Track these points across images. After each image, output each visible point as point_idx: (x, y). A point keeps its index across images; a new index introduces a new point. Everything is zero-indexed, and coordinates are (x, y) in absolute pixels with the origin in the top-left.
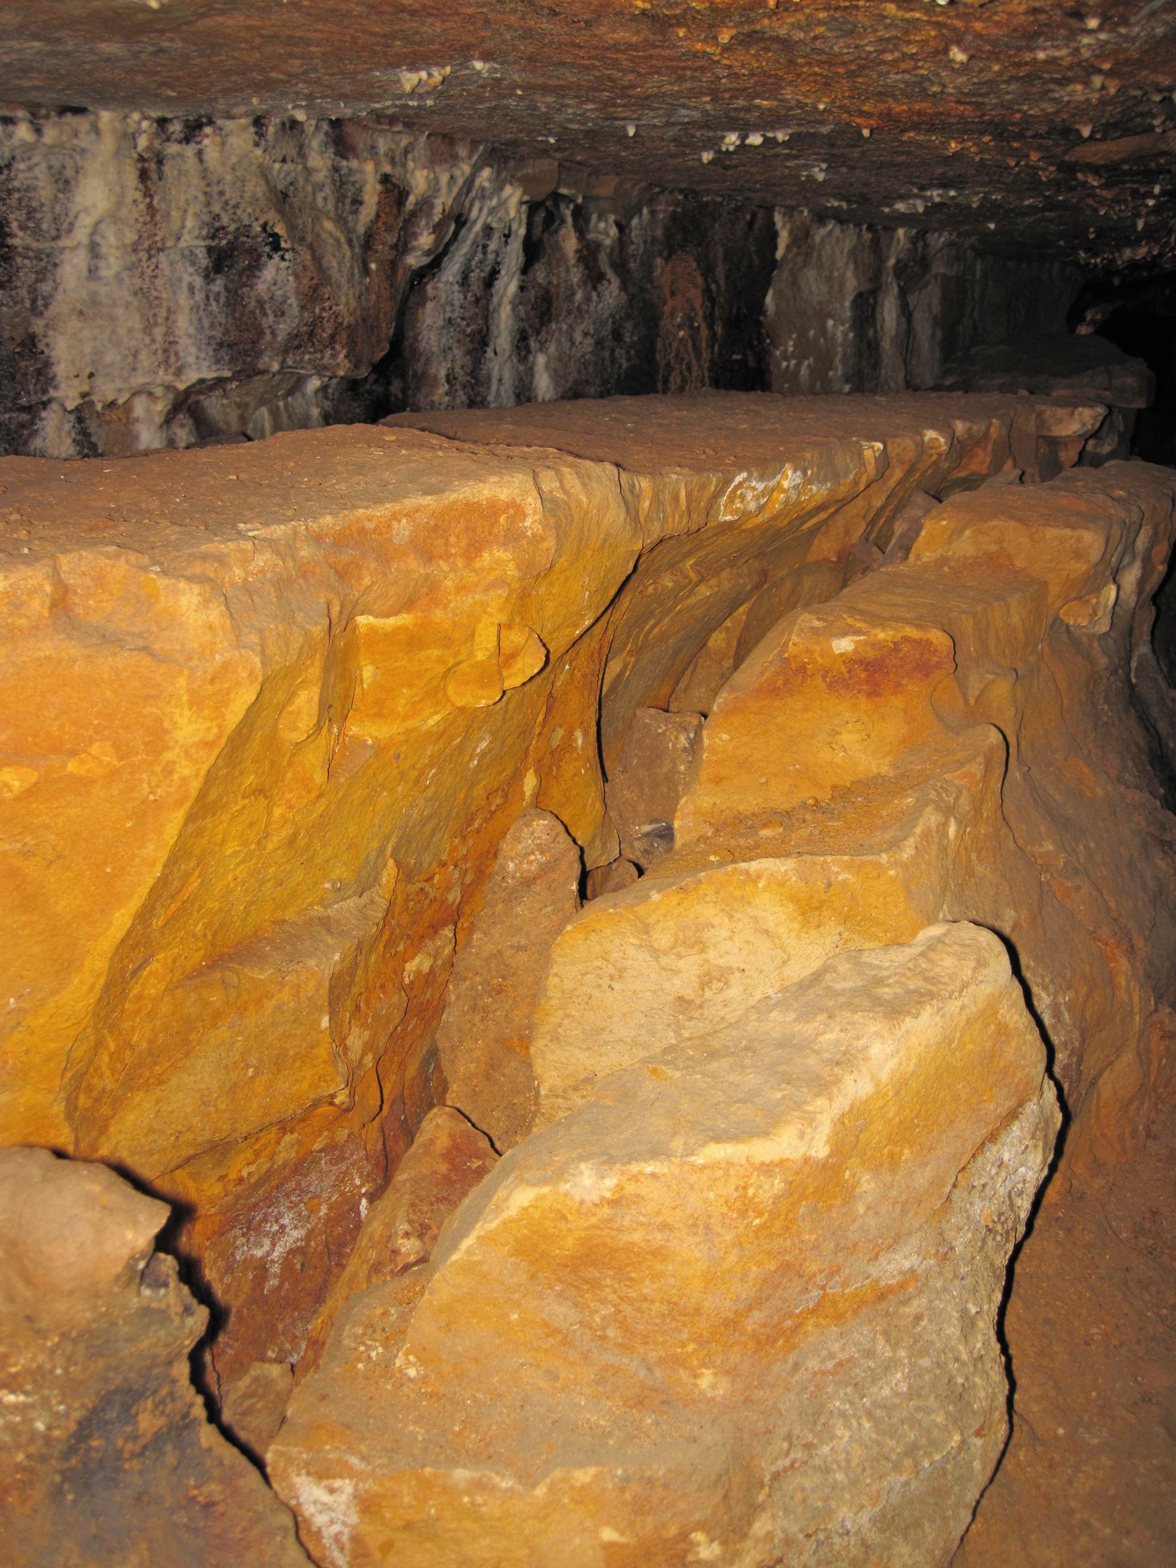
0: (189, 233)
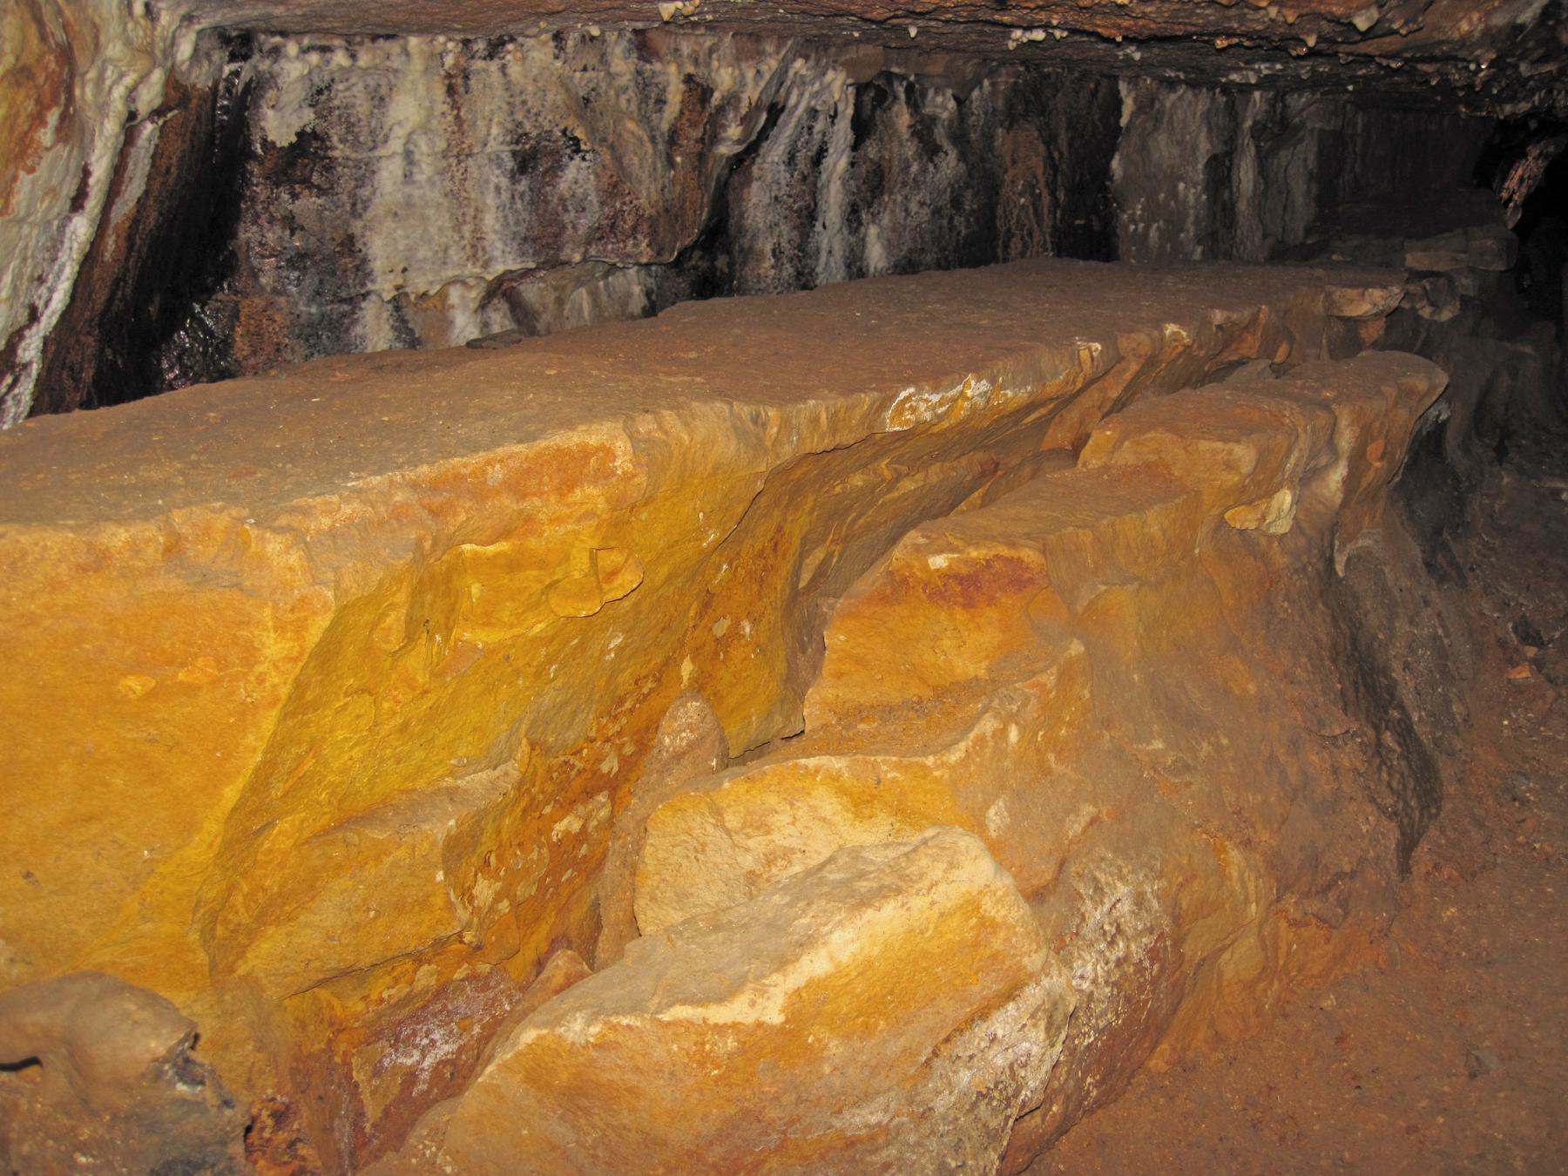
0: (494, 135)
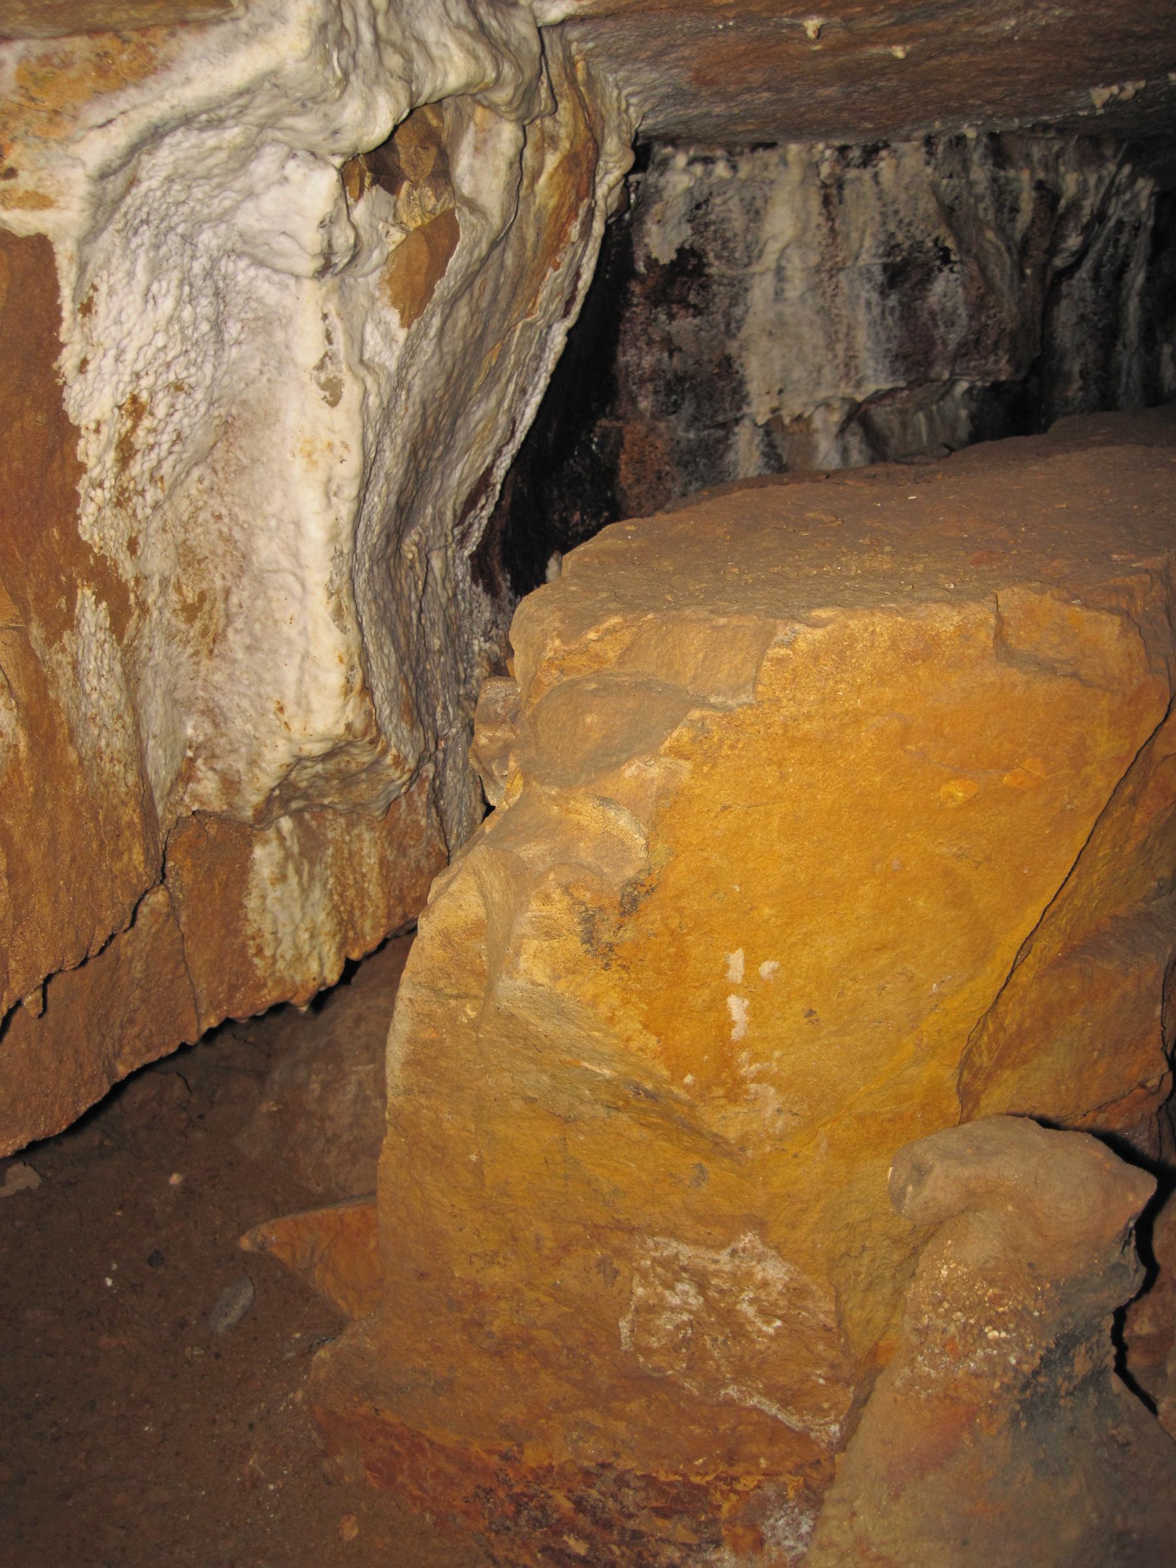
0: (867, 253)
